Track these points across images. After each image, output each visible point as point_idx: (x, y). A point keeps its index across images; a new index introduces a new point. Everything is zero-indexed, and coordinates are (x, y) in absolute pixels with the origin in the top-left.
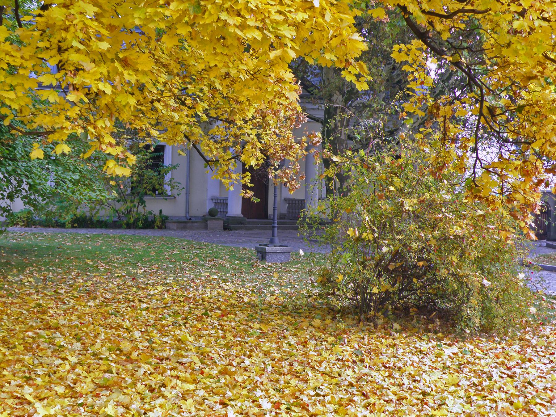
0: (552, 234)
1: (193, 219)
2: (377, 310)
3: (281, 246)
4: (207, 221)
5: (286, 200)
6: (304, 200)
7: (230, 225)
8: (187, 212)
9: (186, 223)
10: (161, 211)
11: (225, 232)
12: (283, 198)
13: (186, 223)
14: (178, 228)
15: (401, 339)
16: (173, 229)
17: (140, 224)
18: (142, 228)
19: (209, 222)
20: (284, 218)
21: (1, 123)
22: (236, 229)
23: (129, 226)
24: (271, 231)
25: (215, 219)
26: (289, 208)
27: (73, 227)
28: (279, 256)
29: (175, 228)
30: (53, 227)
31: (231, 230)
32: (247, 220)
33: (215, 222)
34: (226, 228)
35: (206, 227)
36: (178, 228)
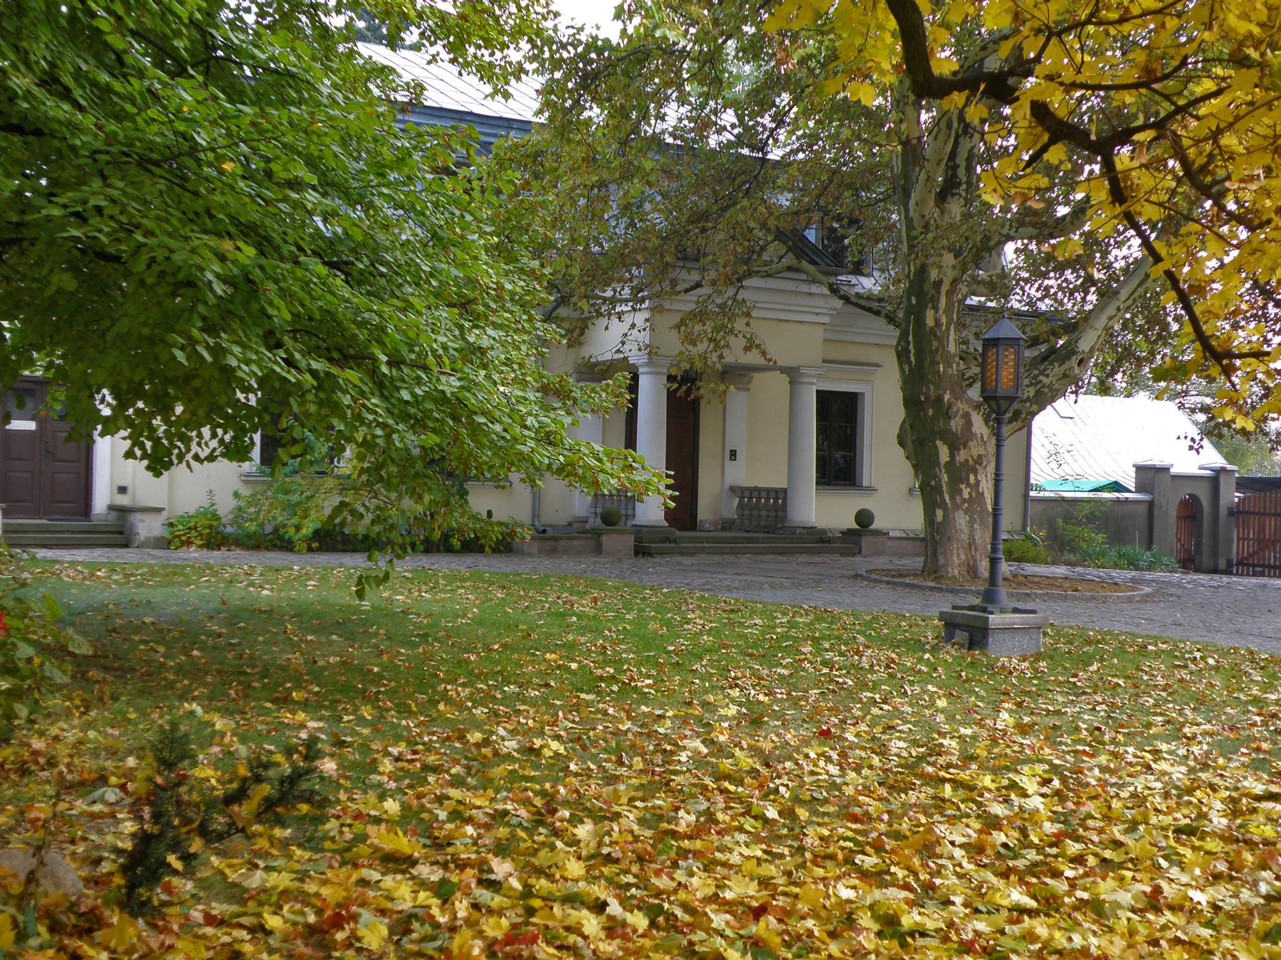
0: (1205, 559)
1: (550, 533)
2: (1078, 729)
3: (1016, 611)
4: (600, 535)
5: (733, 490)
6: (785, 491)
7: (646, 545)
8: (535, 515)
9: (553, 539)
10: (490, 514)
11: (641, 561)
12: (727, 487)
13: (553, 539)
14: (540, 552)
15: (105, 596)
16: (531, 555)
17: (456, 543)
18: (458, 552)
19: (604, 538)
20: (730, 529)
21: (882, 5)
22: (660, 554)
23: (430, 547)
24: (139, 516)
25: (617, 532)
26: (740, 506)
27: (310, 550)
28: (1018, 637)
29: (535, 551)
30: (267, 549)
31: (650, 555)
32: (679, 534)
33: (618, 538)
34: (641, 551)
35: (598, 550)
36: (540, 552)
